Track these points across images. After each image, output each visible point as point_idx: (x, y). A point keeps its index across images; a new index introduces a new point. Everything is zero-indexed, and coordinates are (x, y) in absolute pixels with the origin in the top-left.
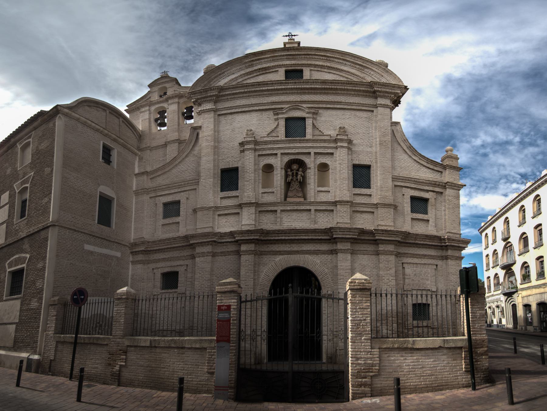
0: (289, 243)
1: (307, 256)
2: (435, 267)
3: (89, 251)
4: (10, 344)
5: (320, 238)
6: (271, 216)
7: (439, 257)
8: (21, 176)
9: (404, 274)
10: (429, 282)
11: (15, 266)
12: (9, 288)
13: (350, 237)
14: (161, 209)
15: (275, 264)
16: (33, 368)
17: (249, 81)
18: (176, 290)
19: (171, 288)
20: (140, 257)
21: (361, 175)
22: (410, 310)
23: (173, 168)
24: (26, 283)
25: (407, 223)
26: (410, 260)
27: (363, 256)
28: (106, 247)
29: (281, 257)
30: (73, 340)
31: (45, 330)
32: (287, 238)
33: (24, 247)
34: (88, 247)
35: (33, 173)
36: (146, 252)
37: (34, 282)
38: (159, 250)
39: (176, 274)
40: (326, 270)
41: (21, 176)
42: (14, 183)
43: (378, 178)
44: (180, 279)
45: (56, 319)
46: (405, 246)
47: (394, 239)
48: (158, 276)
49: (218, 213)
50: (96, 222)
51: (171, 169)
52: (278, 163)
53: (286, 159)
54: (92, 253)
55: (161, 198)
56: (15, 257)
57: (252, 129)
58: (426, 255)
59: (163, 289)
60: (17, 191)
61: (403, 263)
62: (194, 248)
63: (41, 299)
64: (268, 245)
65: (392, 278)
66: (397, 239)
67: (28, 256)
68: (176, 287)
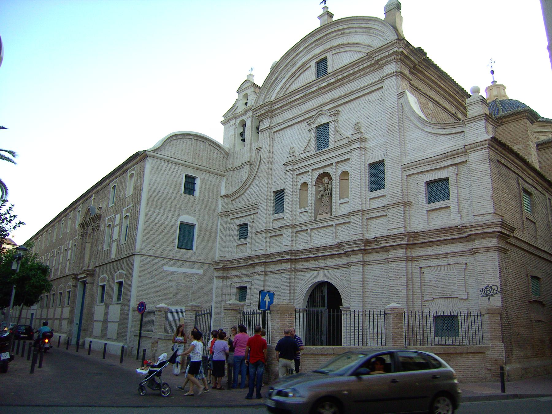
0: (317, 260)
1: (330, 270)
2: (464, 266)
3: (169, 271)
4: (115, 337)
5: (337, 253)
6: (304, 235)
7: (465, 252)
9: (422, 281)
10: (456, 288)
13: (357, 249)
15: (307, 280)
17: (294, 87)
21: (376, 173)
22: (430, 324)
23: (245, 191)
25: (420, 220)
26: (429, 263)
27: (376, 266)
28: (186, 267)
34: (167, 268)
40: (345, 283)
43: (391, 174)
46: (421, 247)
47: (399, 243)
48: (234, 290)
51: (244, 192)
52: (310, 179)
53: (316, 174)
54: (172, 272)
55: (236, 220)
57: (294, 146)
58: (447, 254)
61: (421, 268)
64: (303, 263)
65: (403, 287)
66: (403, 242)
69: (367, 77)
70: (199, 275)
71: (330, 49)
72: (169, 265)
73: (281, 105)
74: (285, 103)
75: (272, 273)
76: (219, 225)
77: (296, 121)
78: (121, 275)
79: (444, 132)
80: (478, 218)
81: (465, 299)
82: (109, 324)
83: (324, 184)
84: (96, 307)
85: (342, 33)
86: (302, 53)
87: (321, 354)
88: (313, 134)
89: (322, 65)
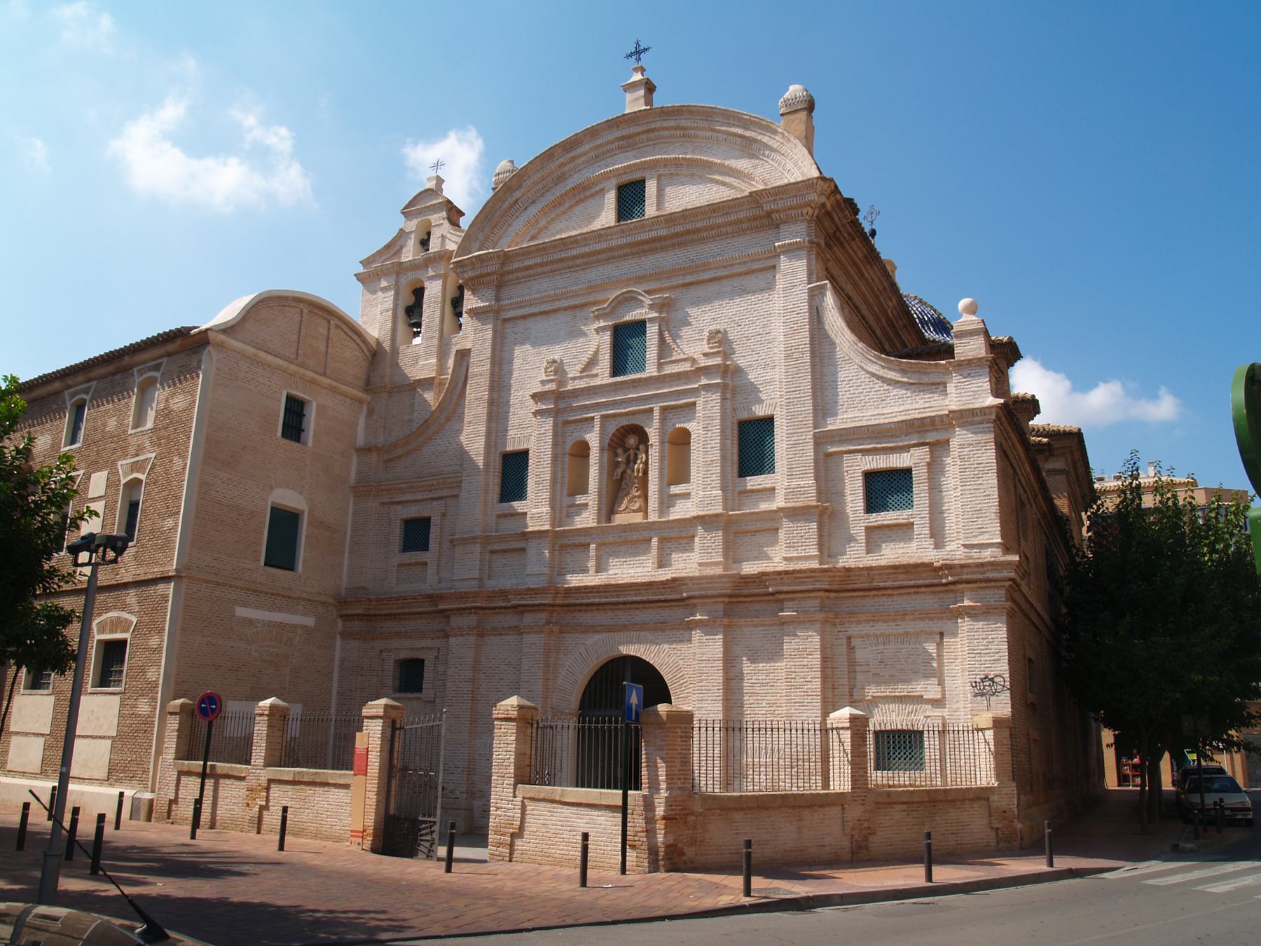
3: (244, 619)
4: (103, 773)
8: (132, 450)
11: (111, 632)
12: (874, 866)
14: (397, 532)
16: (143, 813)
18: (419, 695)
19: (412, 691)
20: (356, 626)
21: (752, 445)
24: (130, 668)
28: (281, 610)
29: (597, 637)
30: (200, 770)
31: (159, 752)
32: (603, 600)
33: (128, 601)
34: (241, 612)
35: (153, 455)
36: (367, 617)
37: (143, 670)
38: (390, 615)
39: (420, 662)
41: (132, 450)
42: (120, 458)
44: (426, 675)
45: (178, 737)
48: (390, 665)
49: (490, 548)
50: (262, 563)
54: (250, 622)
56: (110, 614)
59: (400, 691)
60: (123, 481)
62: (448, 617)
63: (154, 699)
67: (135, 620)
68: (420, 690)
69: (741, 239)
70: (305, 628)
71: (654, 165)
72: (245, 604)
73: (527, 263)
74: (539, 260)
75: (497, 632)
76: (350, 516)
77: (565, 303)
78: (117, 624)
79: (882, 372)
80: (974, 553)
81: (936, 701)
82: (77, 742)
83: (626, 450)
84: (82, 698)
85: (685, 136)
86: (585, 158)
87: (736, 809)
88: (607, 338)
89: (630, 197)
